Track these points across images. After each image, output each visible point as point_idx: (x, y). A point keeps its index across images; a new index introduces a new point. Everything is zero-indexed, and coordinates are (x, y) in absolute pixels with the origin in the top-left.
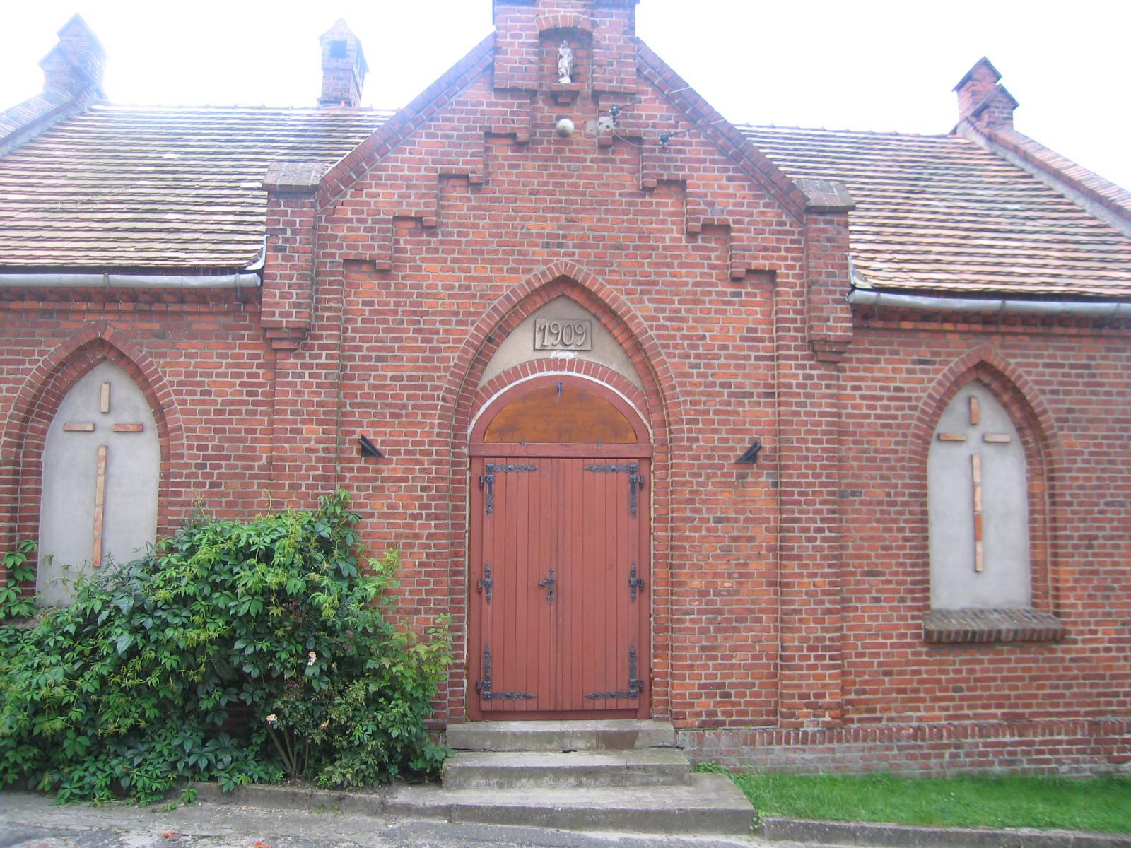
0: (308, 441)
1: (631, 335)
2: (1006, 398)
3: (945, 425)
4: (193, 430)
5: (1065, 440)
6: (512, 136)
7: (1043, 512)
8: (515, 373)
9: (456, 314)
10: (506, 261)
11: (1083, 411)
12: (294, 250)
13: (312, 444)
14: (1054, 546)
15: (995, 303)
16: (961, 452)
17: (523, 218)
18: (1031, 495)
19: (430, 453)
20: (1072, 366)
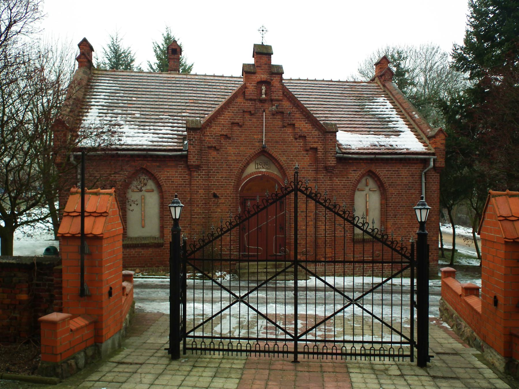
0: (200, 194)
1: (280, 165)
2: (376, 179)
3: (359, 186)
4: (169, 191)
5: (391, 190)
6: (250, 112)
7: (384, 208)
8: (251, 175)
9: (236, 160)
10: (249, 146)
11: (396, 183)
12: (195, 145)
13: (202, 195)
14: (387, 217)
15: (373, 156)
16: (364, 193)
17: (253, 135)
18: (381, 204)
19: (231, 196)
20: (393, 171)
